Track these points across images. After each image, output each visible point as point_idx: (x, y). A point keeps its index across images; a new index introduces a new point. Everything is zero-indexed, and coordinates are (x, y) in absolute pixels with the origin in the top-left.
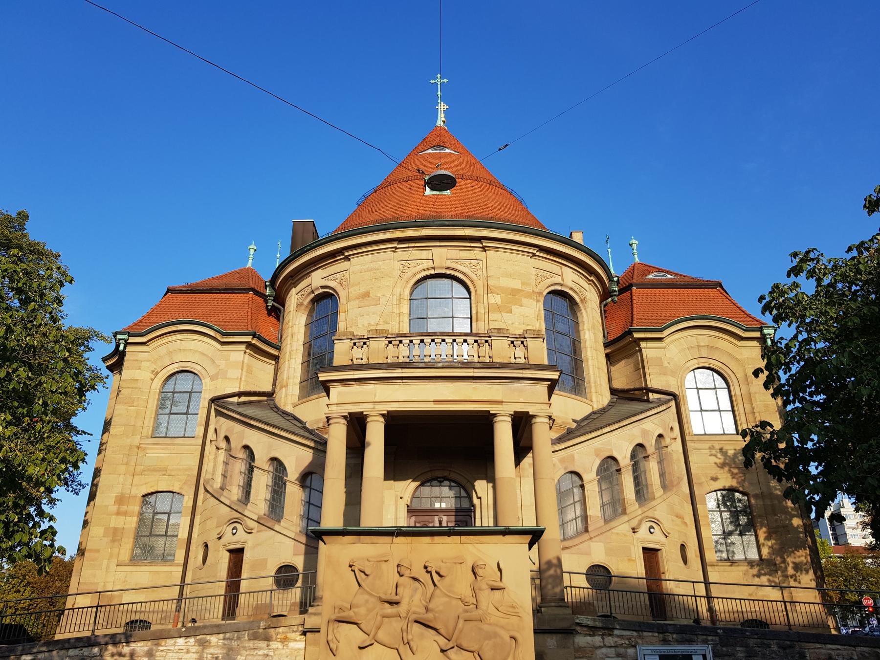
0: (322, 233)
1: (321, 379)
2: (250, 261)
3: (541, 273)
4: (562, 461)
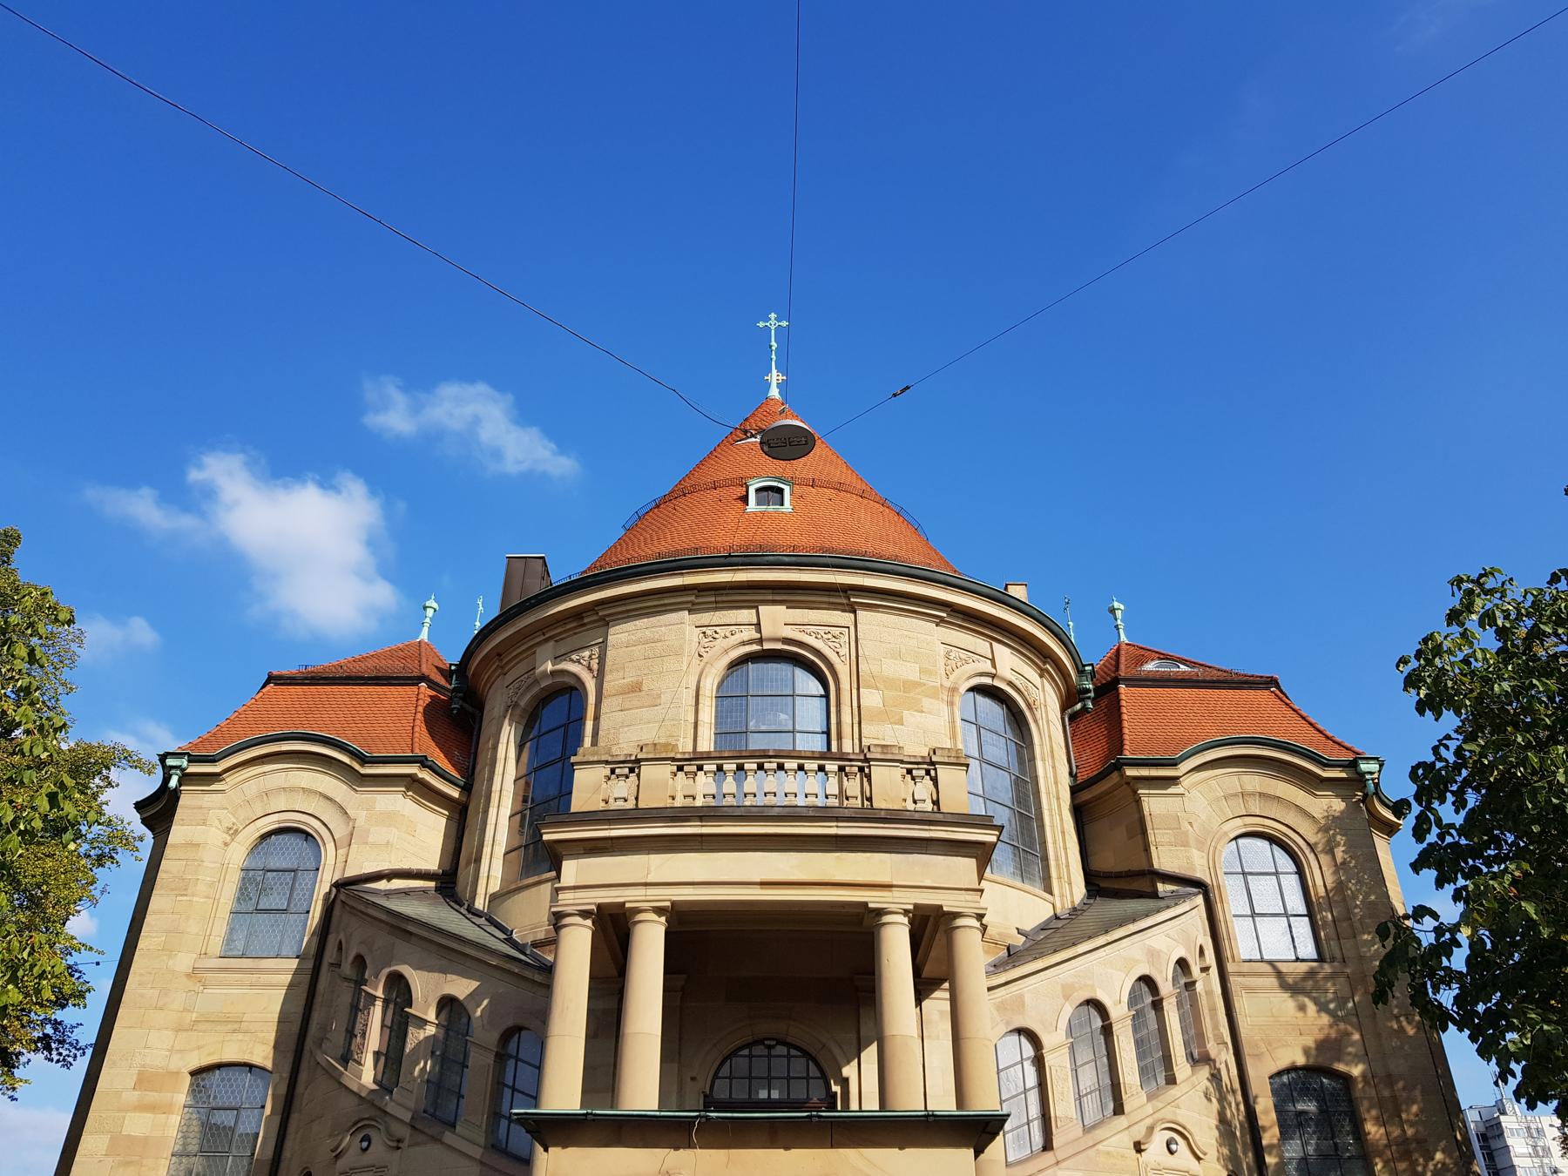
0: (558, 577)
1: (545, 837)
2: (425, 630)
3: (955, 653)
4: (1001, 1007)
